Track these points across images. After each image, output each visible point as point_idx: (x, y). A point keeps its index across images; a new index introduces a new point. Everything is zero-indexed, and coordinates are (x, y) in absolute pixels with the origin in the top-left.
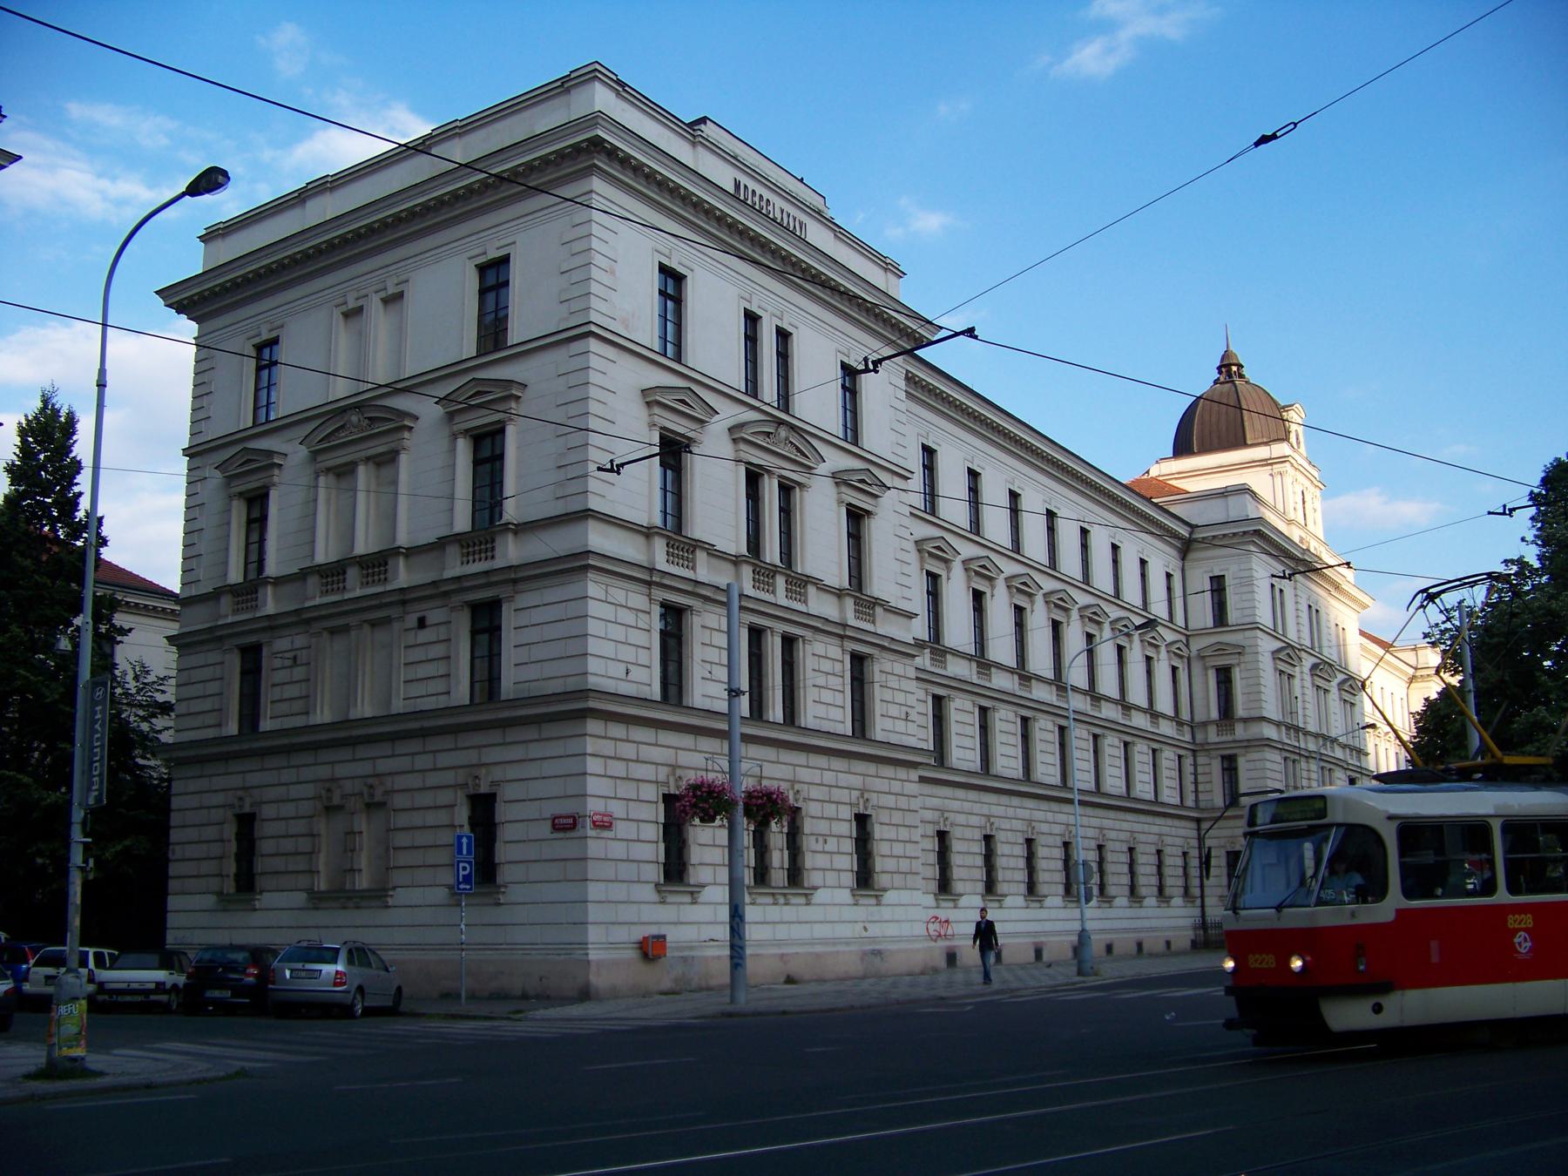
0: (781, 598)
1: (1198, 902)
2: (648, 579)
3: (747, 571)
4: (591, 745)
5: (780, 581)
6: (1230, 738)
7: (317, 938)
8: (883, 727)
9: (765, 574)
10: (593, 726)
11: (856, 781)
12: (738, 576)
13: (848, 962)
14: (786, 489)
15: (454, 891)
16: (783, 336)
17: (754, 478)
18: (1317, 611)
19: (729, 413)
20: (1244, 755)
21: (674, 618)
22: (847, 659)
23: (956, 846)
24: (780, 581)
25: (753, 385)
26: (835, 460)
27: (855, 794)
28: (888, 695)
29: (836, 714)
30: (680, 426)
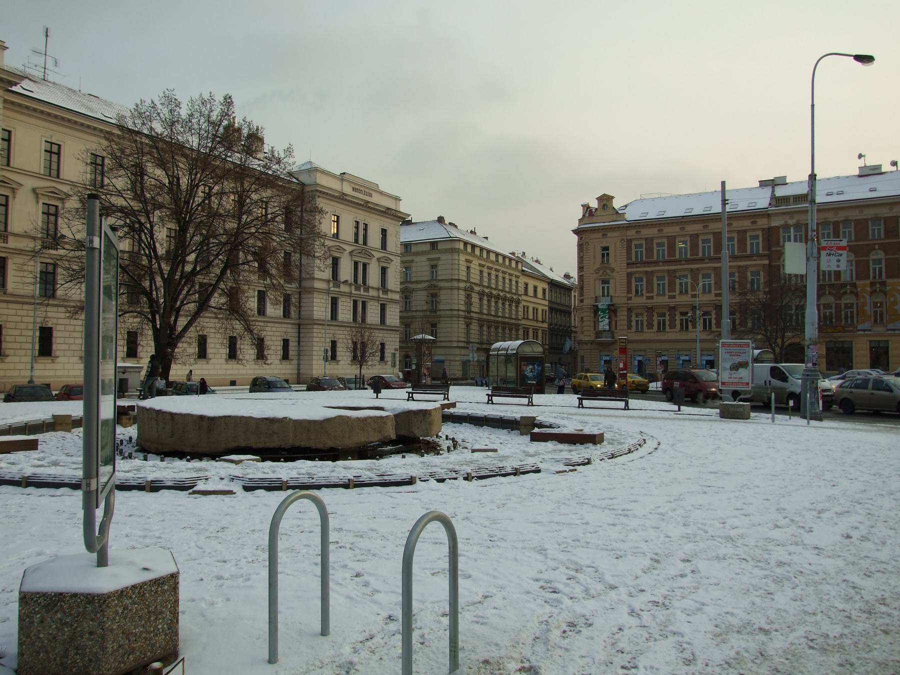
0: (362, 292)
1: (295, 362)
2: (328, 291)
3: (353, 288)
4: (315, 330)
5: (362, 289)
6: (386, 297)
7: (328, 367)
8: (389, 321)
9: (358, 288)
10: (315, 326)
11: (332, 332)
12: (379, 293)
13: (74, 383)
14: (365, 265)
15: (226, 360)
16: (366, 225)
17: (356, 264)
18: (537, 261)
19: (349, 248)
20: (12, 259)
21: (334, 302)
22: (352, 302)
23: (338, 345)
24: (362, 289)
25: (356, 241)
26: (377, 255)
27: (42, 319)
28: (372, 311)
29: (348, 316)
30: (385, 265)
